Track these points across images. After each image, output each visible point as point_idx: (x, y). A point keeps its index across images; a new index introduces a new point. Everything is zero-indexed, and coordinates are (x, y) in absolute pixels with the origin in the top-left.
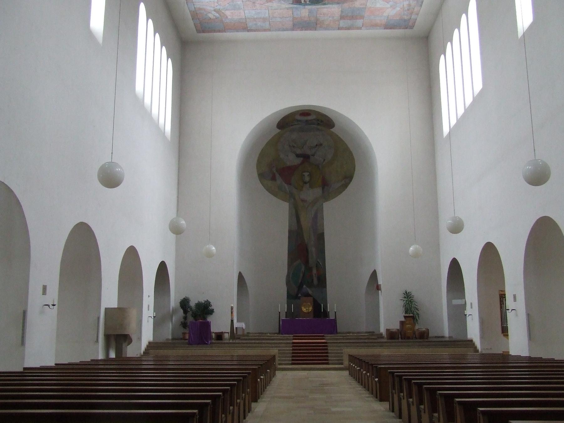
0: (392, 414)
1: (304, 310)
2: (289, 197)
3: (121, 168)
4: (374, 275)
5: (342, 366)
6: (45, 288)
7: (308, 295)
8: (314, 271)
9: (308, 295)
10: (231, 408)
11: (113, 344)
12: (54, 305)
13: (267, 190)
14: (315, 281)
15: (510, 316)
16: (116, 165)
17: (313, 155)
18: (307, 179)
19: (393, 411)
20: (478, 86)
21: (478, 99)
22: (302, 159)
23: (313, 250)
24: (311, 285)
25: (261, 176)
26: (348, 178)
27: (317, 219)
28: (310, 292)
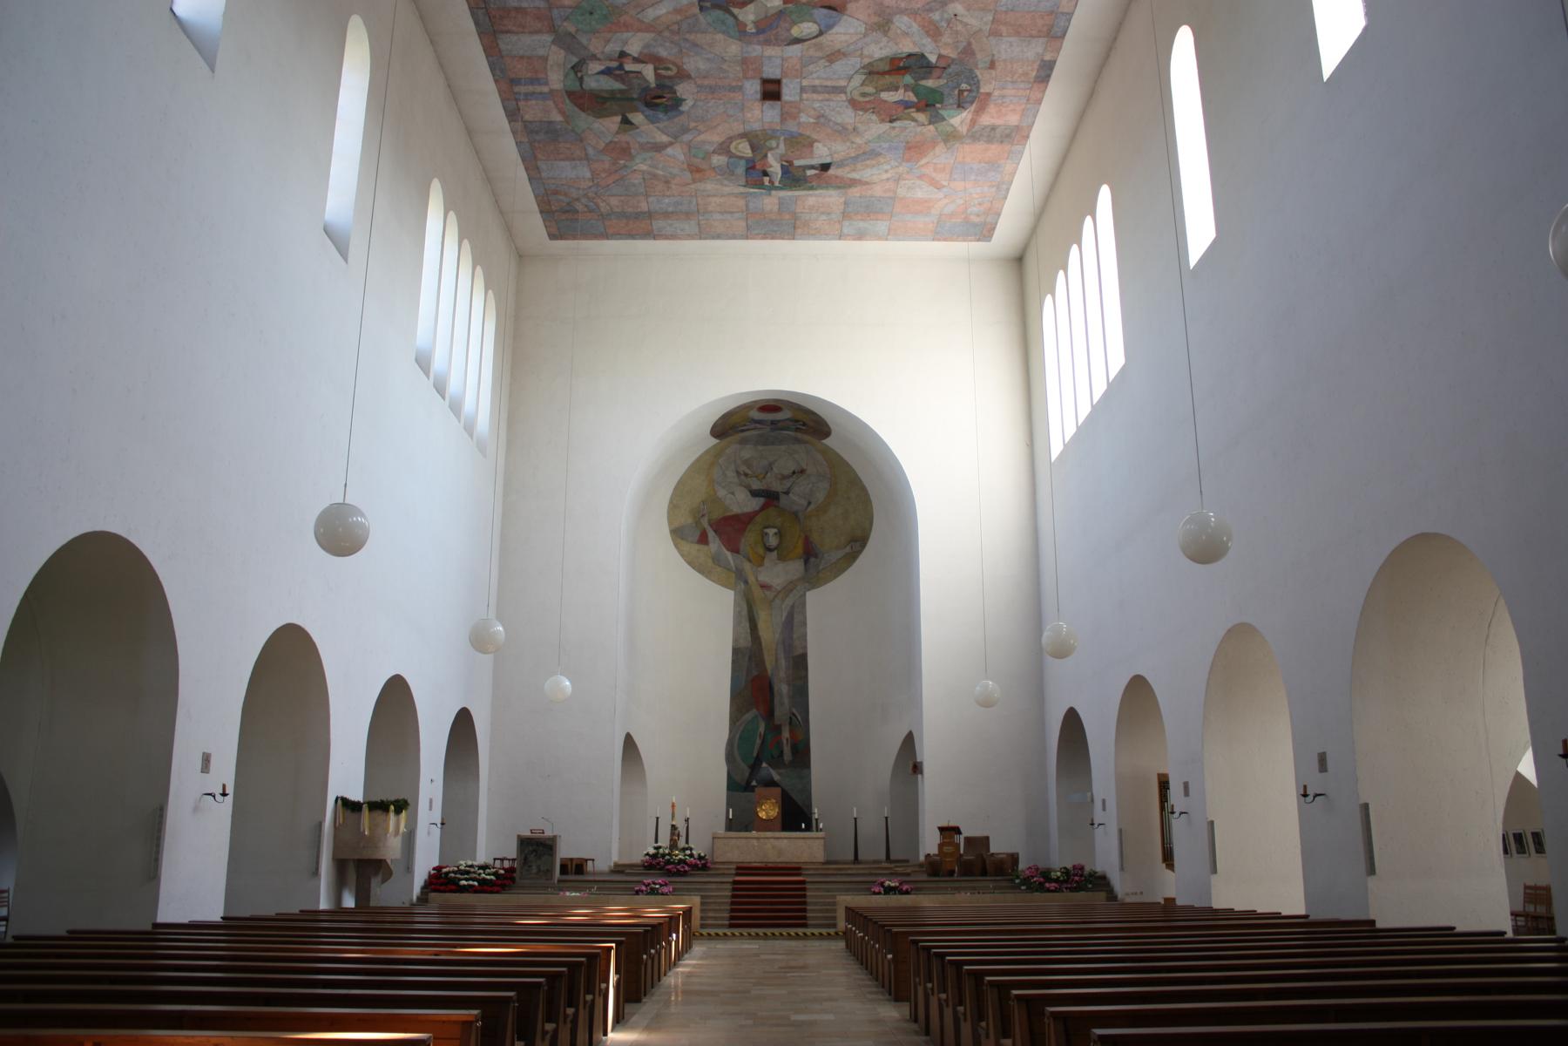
0: (915, 1026)
1: (762, 815)
2: (737, 580)
3: (362, 515)
4: (909, 742)
5: (832, 931)
6: (206, 759)
7: (771, 783)
8: (786, 734)
9: (771, 783)
10: (570, 1011)
11: (352, 876)
12: (224, 794)
13: (690, 563)
14: (788, 755)
15: (1177, 824)
16: (355, 511)
17: (787, 493)
18: (773, 541)
19: (916, 1021)
20: (1118, 360)
21: (1116, 387)
22: (762, 500)
23: (782, 689)
24: (777, 761)
25: (677, 533)
26: (857, 542)
27: (793, 624)
28: (776, 777)
